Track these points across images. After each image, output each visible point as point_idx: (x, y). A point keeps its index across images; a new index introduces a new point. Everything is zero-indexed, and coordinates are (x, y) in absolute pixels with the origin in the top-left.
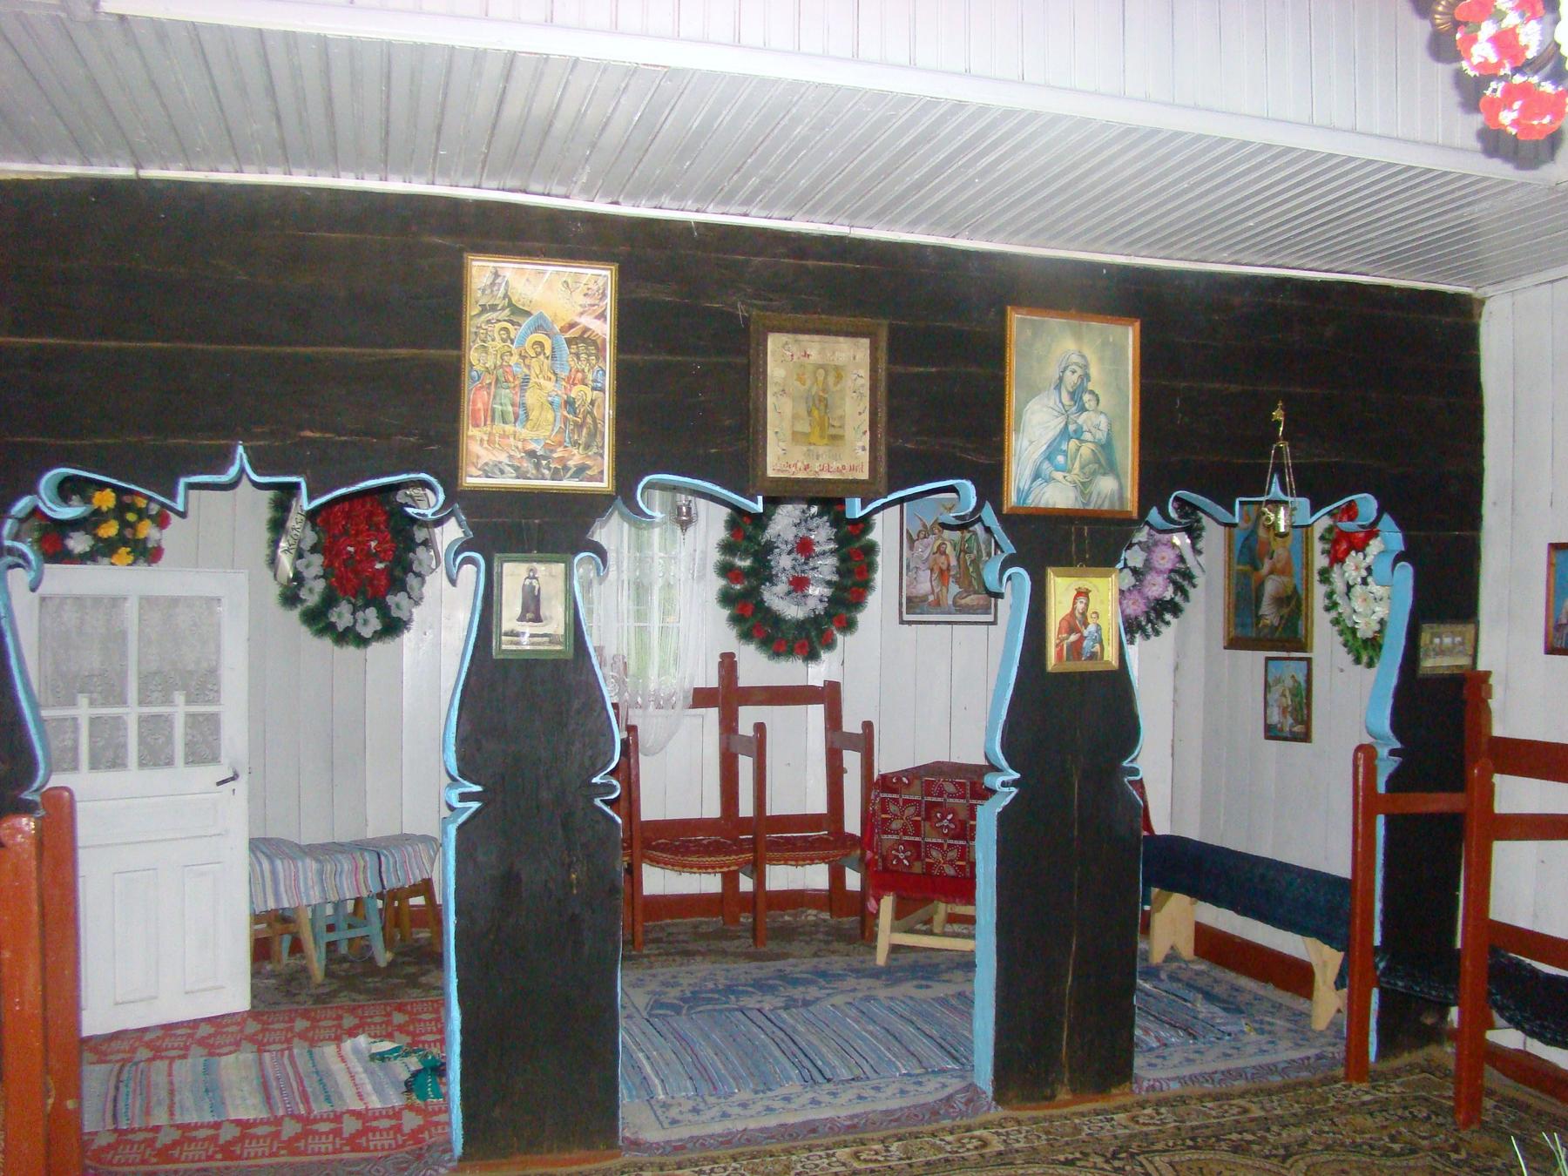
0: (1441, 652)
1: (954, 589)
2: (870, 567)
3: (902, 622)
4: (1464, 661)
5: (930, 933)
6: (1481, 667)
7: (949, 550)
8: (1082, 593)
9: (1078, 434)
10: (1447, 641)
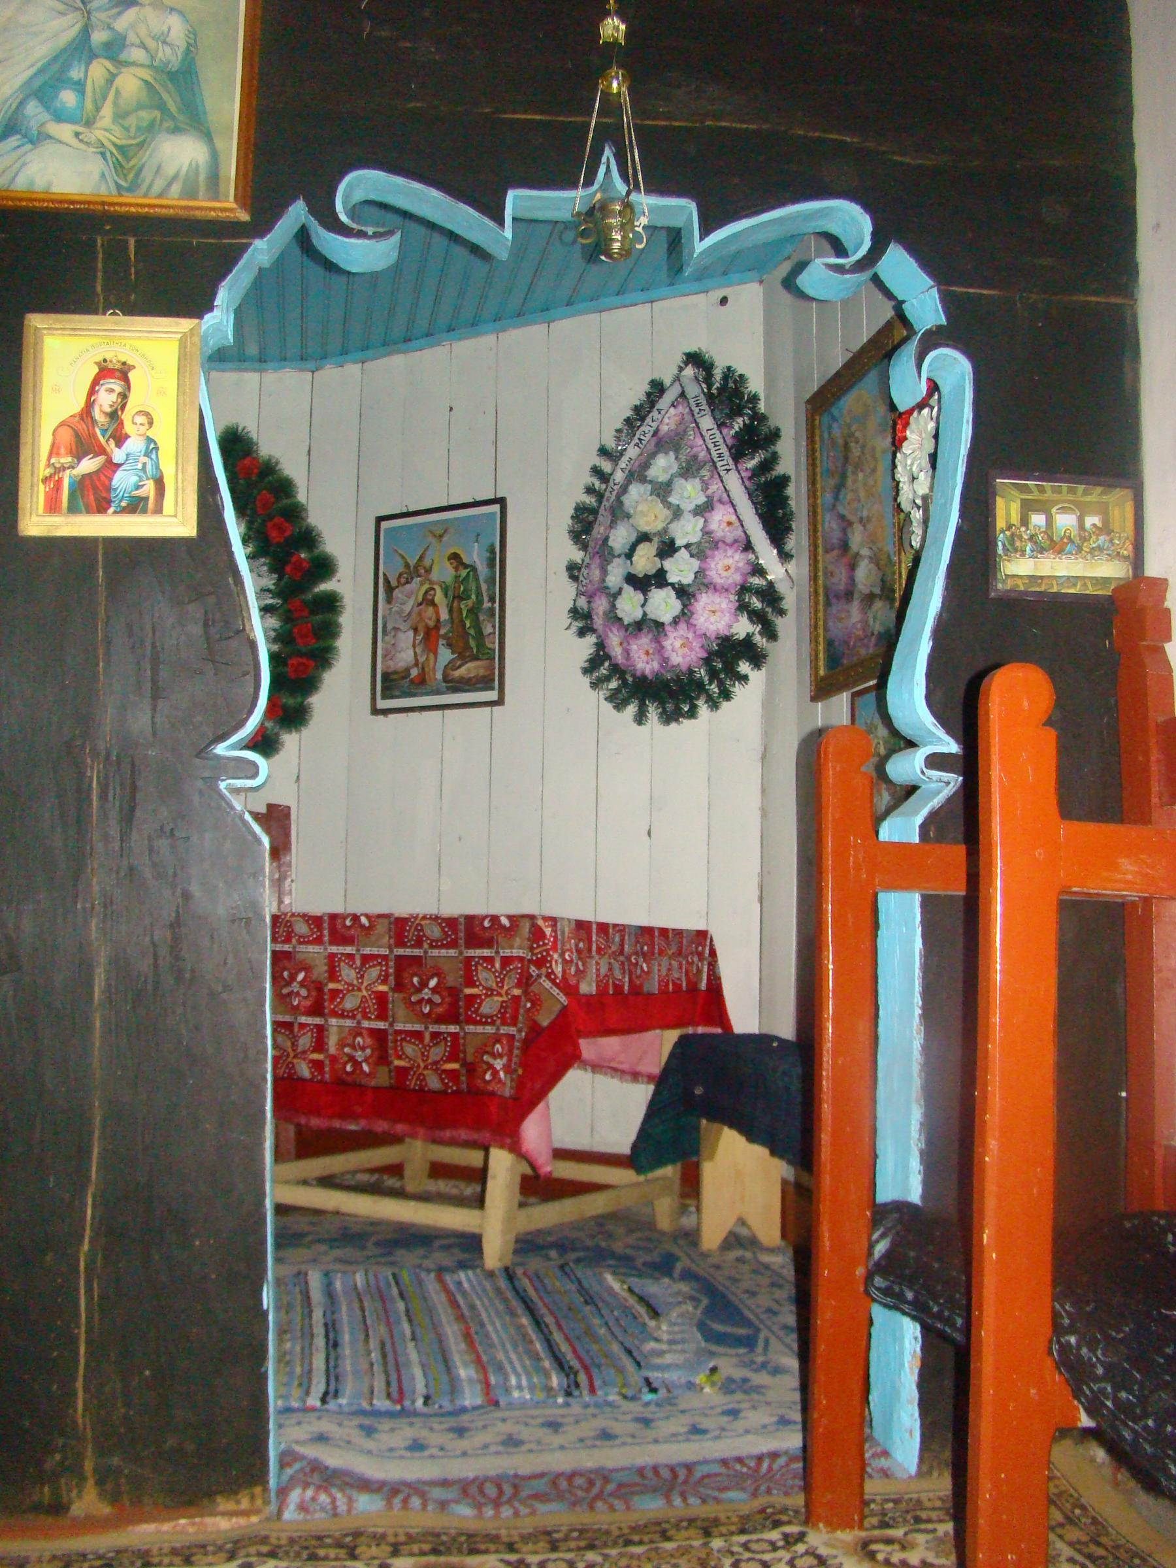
0: (1054, 545)
1: (445, 655)
2: (330, 630)
3: (376, 711)
4: (1112, 570)
5: (399, 1194)
6: (1152, 569)
7: (439, 597)
8: (114, 372)
9: (114, 49)
10: (1065, 522)
